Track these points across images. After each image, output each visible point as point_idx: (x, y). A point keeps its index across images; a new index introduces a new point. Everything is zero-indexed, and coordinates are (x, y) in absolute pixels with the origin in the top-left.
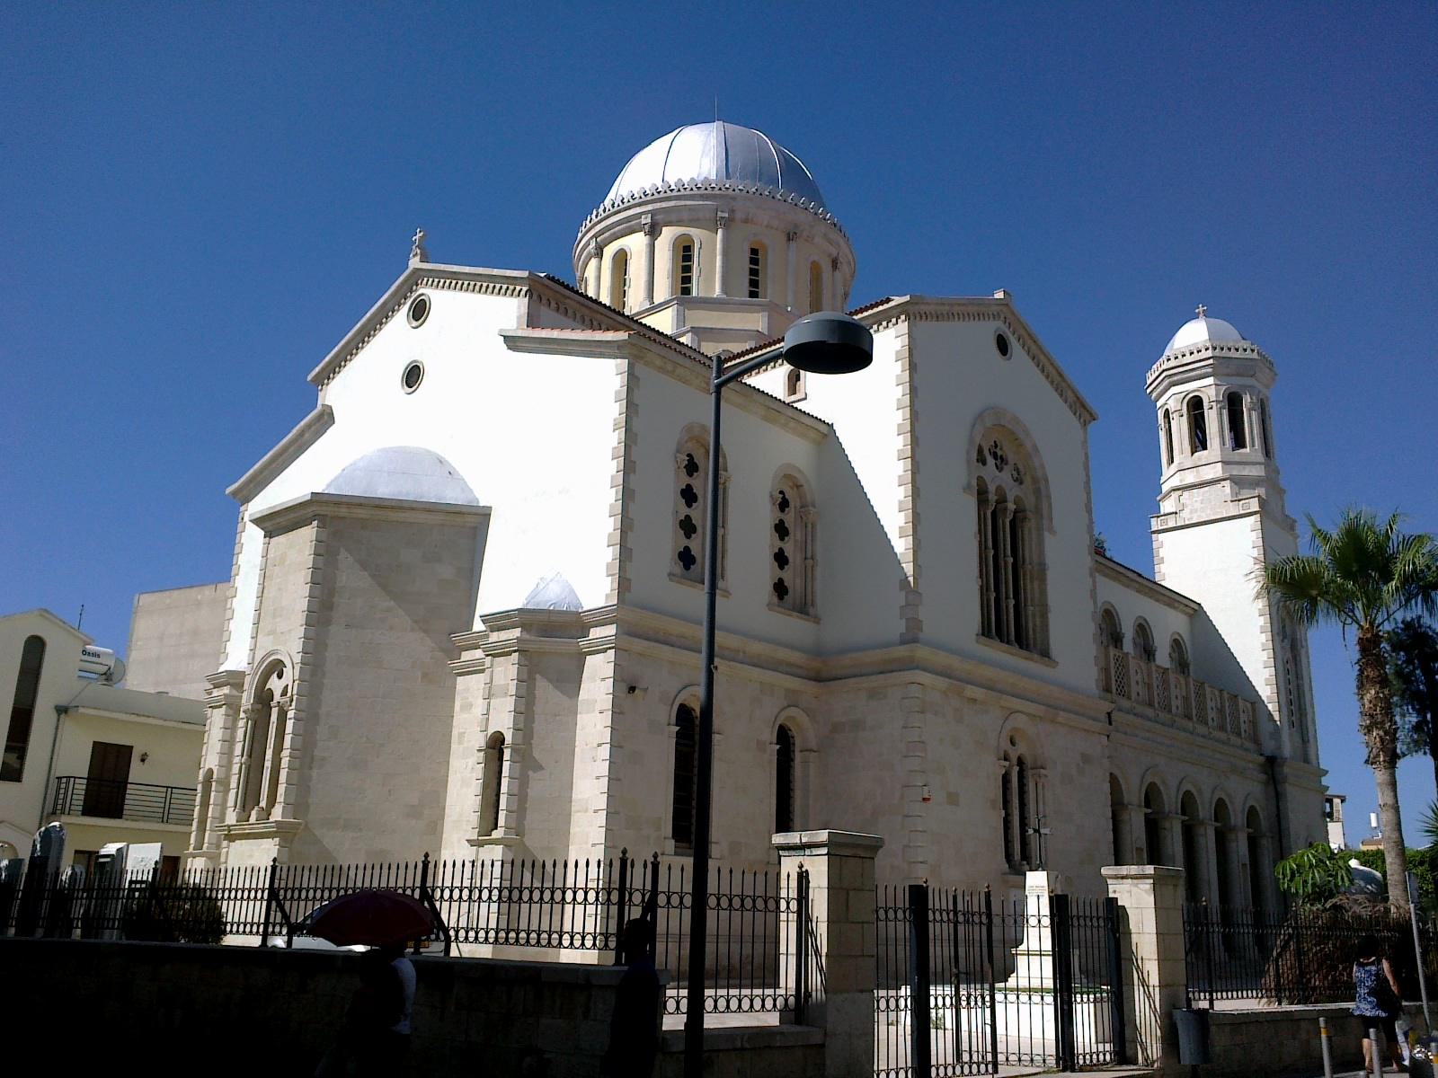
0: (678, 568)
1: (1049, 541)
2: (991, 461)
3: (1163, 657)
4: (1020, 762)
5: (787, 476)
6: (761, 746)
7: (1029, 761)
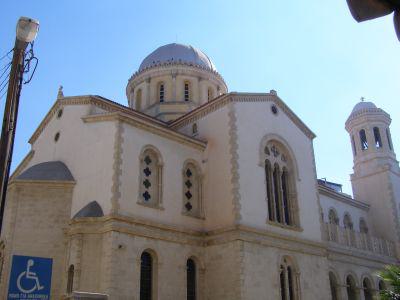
0: (185, 210)
1: (298, 184)
2: (272, 153)
3: (356, 226)
4: (289, 269)
5: (189, 164)
6: (276, 286)
7: (292, 268)
